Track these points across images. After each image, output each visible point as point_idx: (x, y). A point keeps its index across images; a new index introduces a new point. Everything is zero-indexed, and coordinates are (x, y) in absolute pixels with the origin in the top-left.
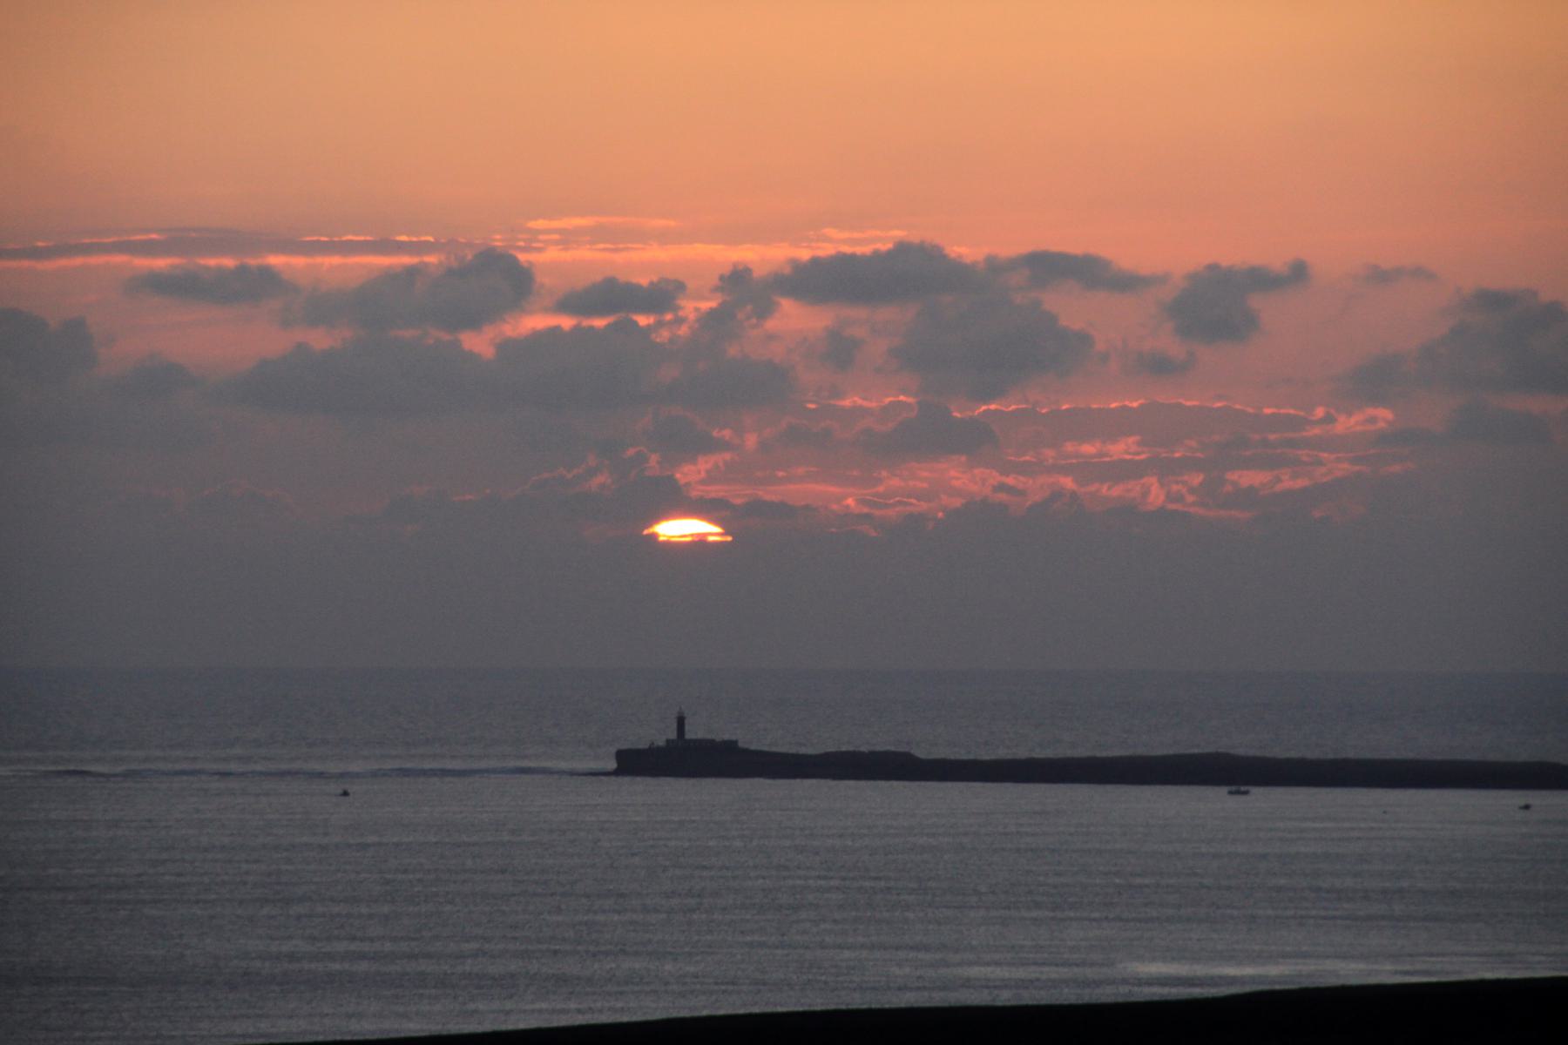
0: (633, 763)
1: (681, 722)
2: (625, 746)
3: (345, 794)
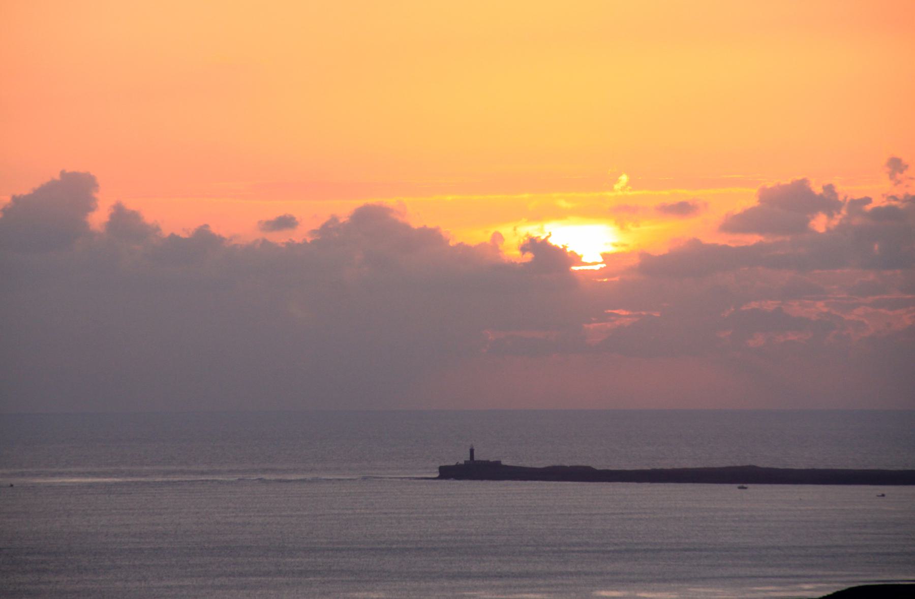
0: (447, 473)
1: (472, 451)
2: (443, 464)
3: (883, 495)
